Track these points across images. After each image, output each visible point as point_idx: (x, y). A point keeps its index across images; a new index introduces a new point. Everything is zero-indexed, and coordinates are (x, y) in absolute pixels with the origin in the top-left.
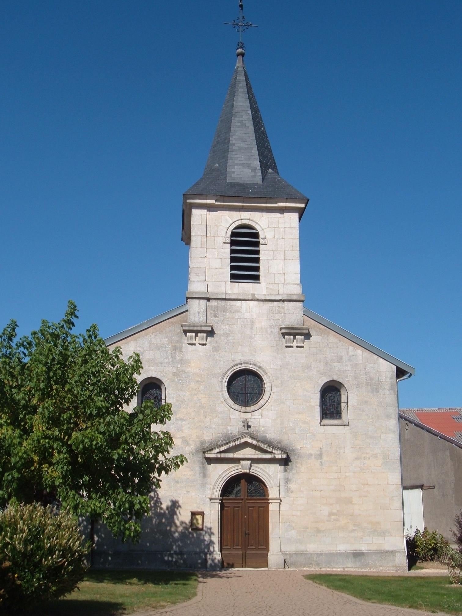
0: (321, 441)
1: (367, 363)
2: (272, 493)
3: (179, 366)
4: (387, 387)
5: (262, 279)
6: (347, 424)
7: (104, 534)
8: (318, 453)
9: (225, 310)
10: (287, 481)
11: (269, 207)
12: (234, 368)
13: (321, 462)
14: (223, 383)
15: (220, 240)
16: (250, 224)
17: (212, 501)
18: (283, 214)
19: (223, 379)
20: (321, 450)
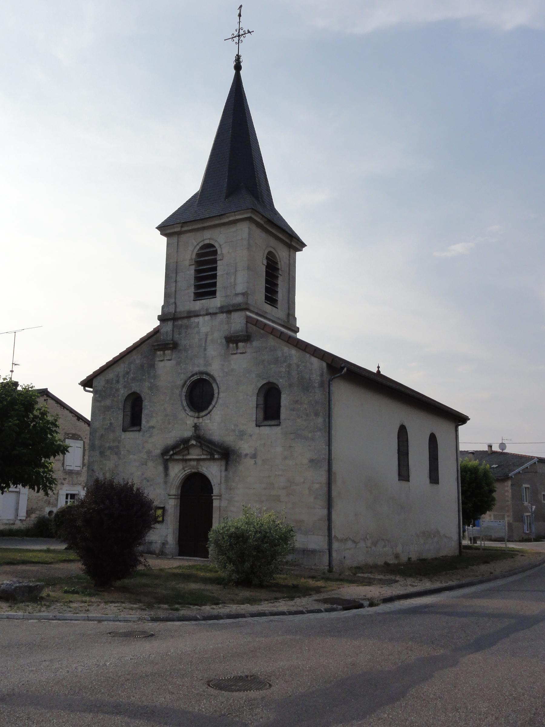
0: (423, 654)
1: (300, 363)
2: (216, 491)
3: (152, 381)
4: (316, 385)
5: (218, 294)
6: (279, 424)
7: (72, 588)
8: (253, 452)
9: (187, 327)
10: (227, 479)
11: (212, 256)
12: (192, 379)
13: (255, 461)
14: (183, 393)
15: (187, 263)
16: (210, 243)
17: (170, 497)
18: (47, 548)
19: (182, 389)
20: (256, 449)
